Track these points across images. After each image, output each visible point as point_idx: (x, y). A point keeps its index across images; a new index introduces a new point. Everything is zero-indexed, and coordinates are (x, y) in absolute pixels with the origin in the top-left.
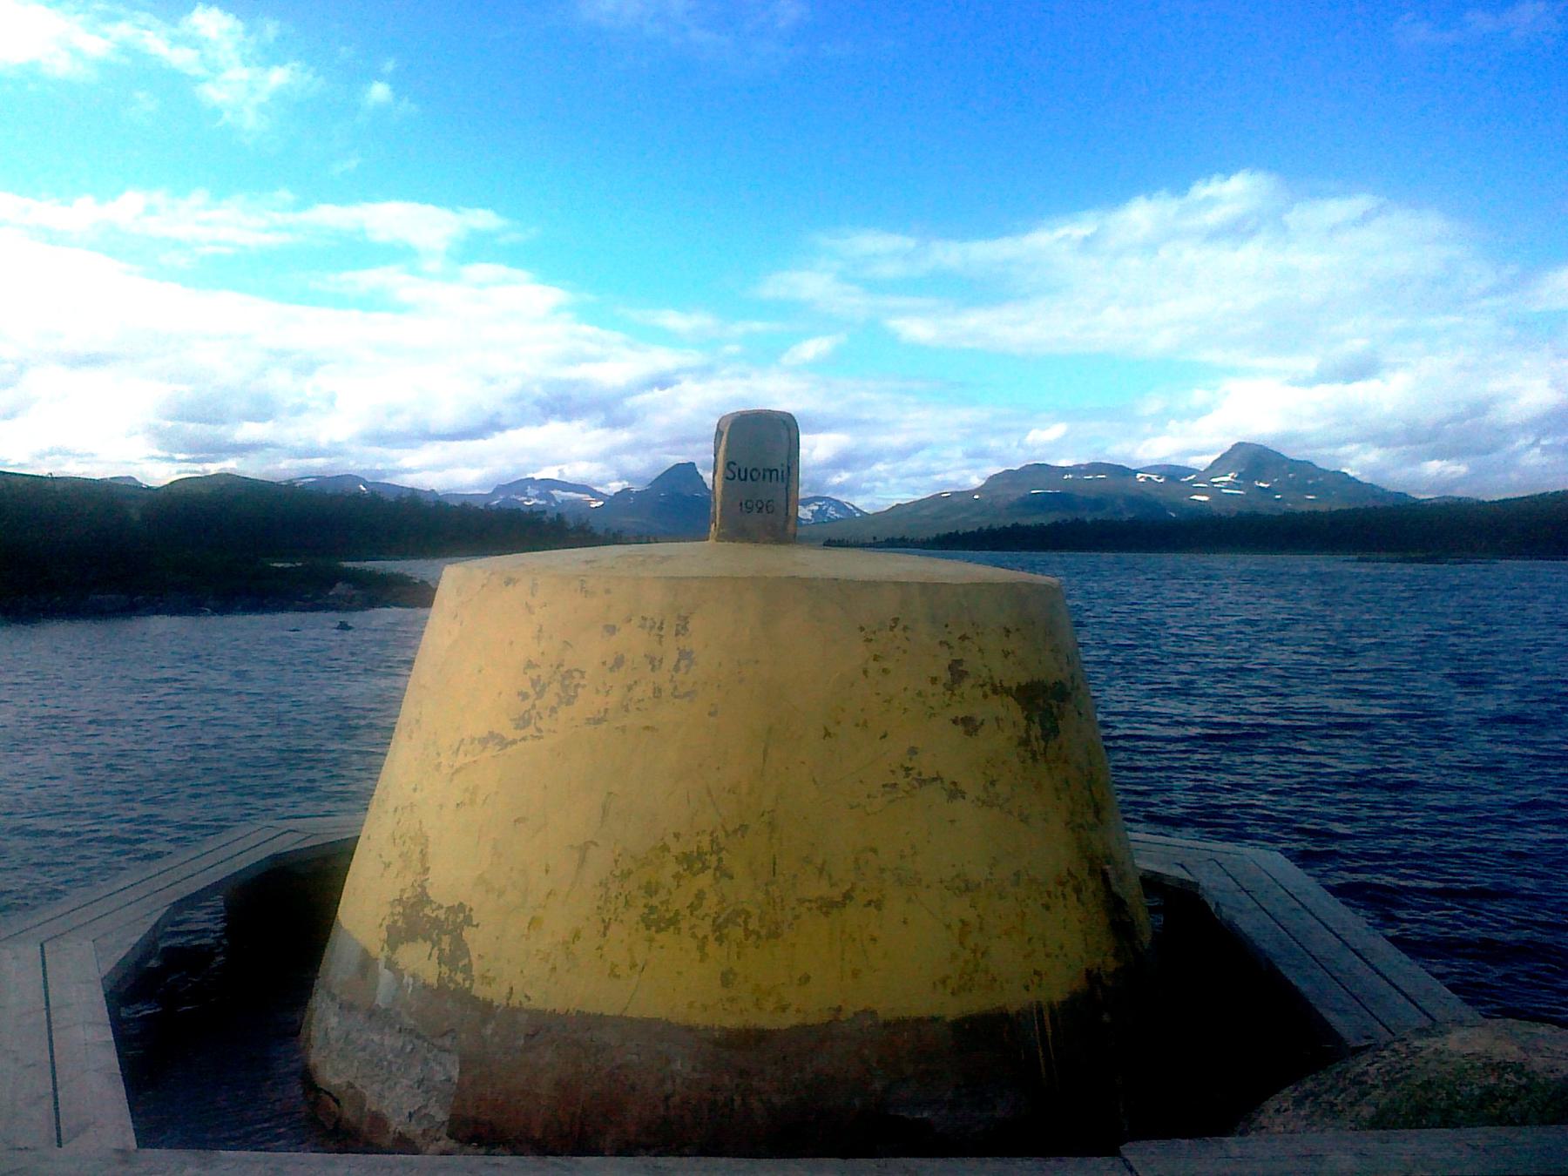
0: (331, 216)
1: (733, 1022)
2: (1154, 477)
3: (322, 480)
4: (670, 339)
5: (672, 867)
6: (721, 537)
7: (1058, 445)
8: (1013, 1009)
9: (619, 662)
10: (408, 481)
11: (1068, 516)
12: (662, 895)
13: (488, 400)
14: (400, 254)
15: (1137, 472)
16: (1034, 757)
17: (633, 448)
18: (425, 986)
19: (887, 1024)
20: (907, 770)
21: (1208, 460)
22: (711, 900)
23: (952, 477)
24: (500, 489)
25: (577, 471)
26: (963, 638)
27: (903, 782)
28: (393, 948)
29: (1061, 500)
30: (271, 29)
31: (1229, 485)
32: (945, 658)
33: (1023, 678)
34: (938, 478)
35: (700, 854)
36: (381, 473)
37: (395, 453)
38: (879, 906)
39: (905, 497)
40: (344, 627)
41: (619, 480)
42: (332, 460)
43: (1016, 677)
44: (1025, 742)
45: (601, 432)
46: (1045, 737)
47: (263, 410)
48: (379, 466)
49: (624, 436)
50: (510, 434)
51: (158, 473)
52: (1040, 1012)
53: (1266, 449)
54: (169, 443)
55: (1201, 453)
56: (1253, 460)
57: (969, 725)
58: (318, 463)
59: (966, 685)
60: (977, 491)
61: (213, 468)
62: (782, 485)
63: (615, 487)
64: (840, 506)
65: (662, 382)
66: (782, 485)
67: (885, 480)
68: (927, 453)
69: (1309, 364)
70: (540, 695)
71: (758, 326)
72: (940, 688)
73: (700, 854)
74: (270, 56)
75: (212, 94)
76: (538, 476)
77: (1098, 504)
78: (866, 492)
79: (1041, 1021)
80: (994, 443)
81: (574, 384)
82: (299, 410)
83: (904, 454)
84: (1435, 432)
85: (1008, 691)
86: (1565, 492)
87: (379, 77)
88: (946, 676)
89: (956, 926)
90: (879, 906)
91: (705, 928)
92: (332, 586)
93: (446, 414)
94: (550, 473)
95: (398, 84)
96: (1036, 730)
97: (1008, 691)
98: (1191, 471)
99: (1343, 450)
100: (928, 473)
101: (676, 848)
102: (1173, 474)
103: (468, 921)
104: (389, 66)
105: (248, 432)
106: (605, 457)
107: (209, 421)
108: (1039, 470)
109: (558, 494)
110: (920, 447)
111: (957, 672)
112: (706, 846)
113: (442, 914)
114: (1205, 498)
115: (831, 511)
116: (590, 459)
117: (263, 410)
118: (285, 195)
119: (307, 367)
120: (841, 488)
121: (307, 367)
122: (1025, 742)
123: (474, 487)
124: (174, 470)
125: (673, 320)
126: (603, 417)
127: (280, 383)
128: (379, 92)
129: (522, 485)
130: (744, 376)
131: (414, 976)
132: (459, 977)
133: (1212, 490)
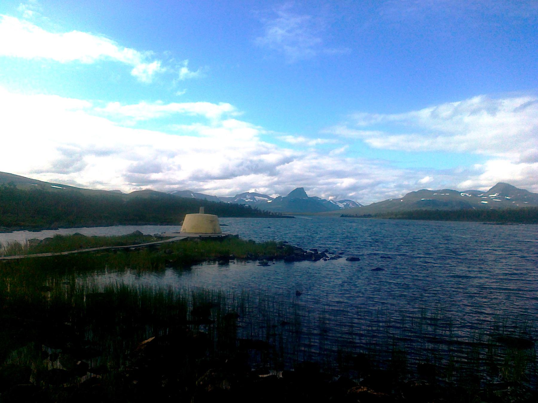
0: (175, 107)
2: (467, 194)
3: (179, 192)
4: (290, 146)
7: (430, 184)
10: (206, 193)
11: (434, 209)
13: (232, 165)
14: (202, 119)
15: (461, 192)
17: (278, 183)
21: (488, 189)
23: (391, 194)
24: (237, 196)
25: (262, 190)
29: (433, 202)
30: (149, 53)
31: (496, 198)
34: (387, 194)
36: (197, 190)
37: (201, 183)
39: (376, 201)
41: (276, 193)
42: (181, 186)
45: (269, 178)
47: (157, 169)
48: (196, 188)
49: (276, 179)
50: (238, 178)
51: (127, 189)
53: (509, 185)
54: (130, 180)
55: (484, 186)
56: (503, 189)
58: (176, 186)
60: (402, 199)
61: (144, 188)
63: (274, 196)
64: (354, 203)
65: (287, 160)
67: (367, 195)
68: (380, 185)
69: (517, 156)
71: (319, 141)
74: (149, 60)
75: (134, 72)
76: (250, 191)
77: (446, 204)
78: (361, 198)
80: (406, 183)
81: (261, 161)
82: (169, 169)
83: (373, 185)
84: (392, 214)
86: (512, 341)
87: (182, 66)
93: (216, 171)
94: (252, 191)
95: (191, 68)
98: (481, 192)
99: (534, 186)
100: (382, 193)
102: (475, 193)
104: (186, 62)
105: (154, 176)
106: (270, 186)
107: (142, 173)
108: (424, 192)
109: (257, 198)
110: (379, 183)
114: (486, 202)
115: (351, 205)
116: (266, 187)
117: (157, 169)
118: (160, 102)
119: (172, 155)
120: (351, 197)
121: (172, 155)
123: (227, 195)
124: (132, 188)
125: (290, 139)
126: (269, 172)
127: (163, 160)
128: (184, 71)
129: (245, 195)
130: (316, 158)
133: (489, 199)
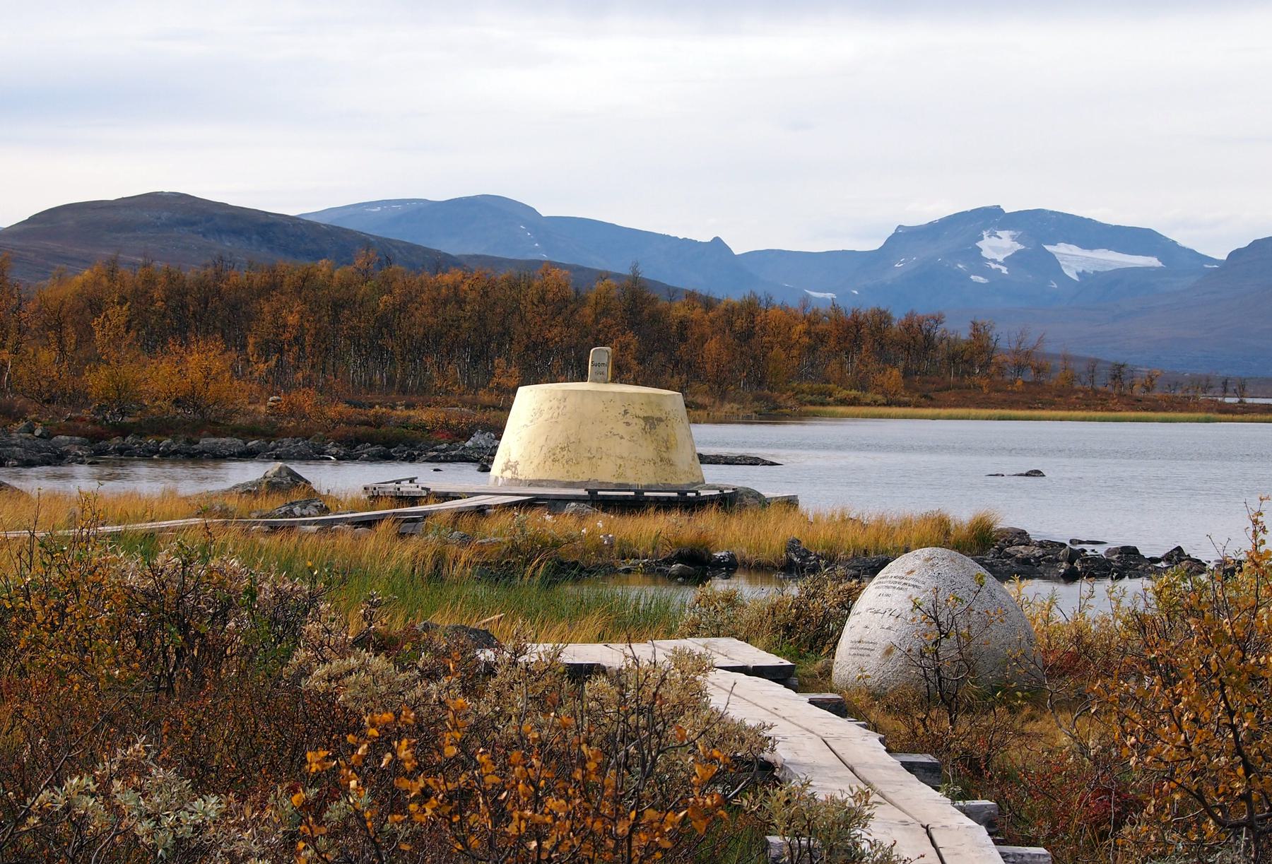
43: (642, 414)
57: (628, 424)
111: (626, 412)
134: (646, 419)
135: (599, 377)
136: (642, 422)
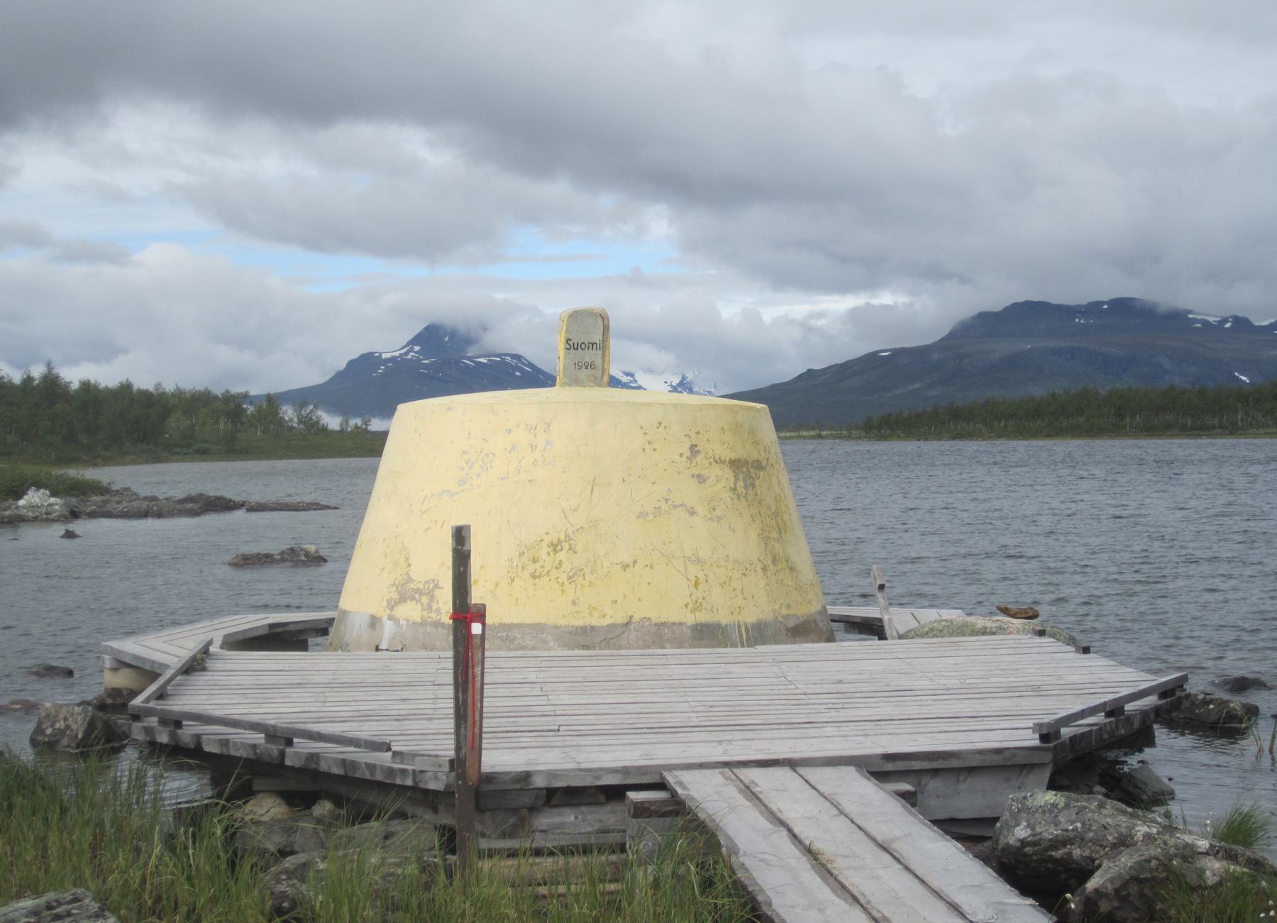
1: (578, 622)
5: (545, 549)
6: (563, 385)
8: (724, 622)
9: (513, 449)
12: (541, 563)
16: (739, 497)
18: (414, 623)
19: (656, 625)
20: (667, 500)
22: (566, 566)
26: (698, 433)
27: (664, 506)
28: (392, 610)
32: (687, 446)
33: (734, 456)
35: (559, 541)
38: (651, 567)
40: (70, 535)
43: (729, 455)
44: (734, 489)
46: (746, 487)
52: (739, 626)
57: (701, 479)
59: (699, 458)
62: (600, 352)
66: (600, 352)
70: (471, 467)
72: (684, 459)
73: (559, 541)
79: (740, 631)
85: (724, 462)
88: (687, 453)
89: (693, 579)
90: (651, 567)
91: (563, 578)
92: (19, 494)
96: (740, 484)
97: (724, 462)
101: (547, 540)
103: (437, 586)
112: (562, 538)
113: (421, 586)
122: (734, 489)
131: (407, 620)
132: (433, 615)
134: (735, 464)
135: (584, 373)
136: (728, 473)
